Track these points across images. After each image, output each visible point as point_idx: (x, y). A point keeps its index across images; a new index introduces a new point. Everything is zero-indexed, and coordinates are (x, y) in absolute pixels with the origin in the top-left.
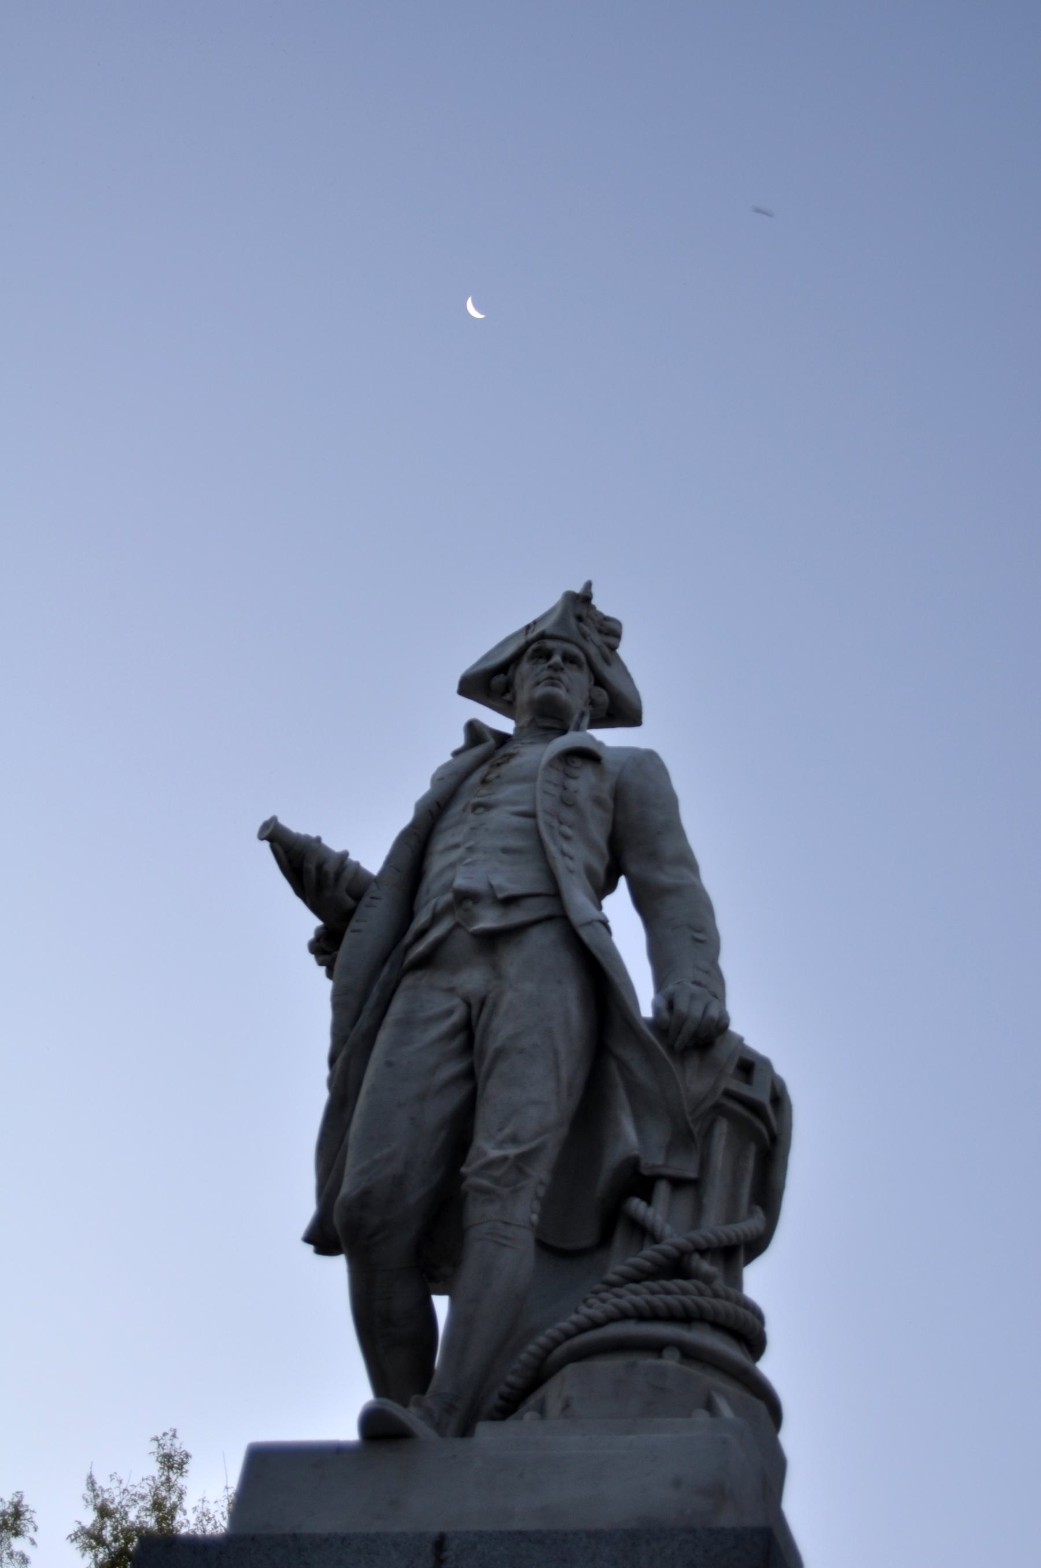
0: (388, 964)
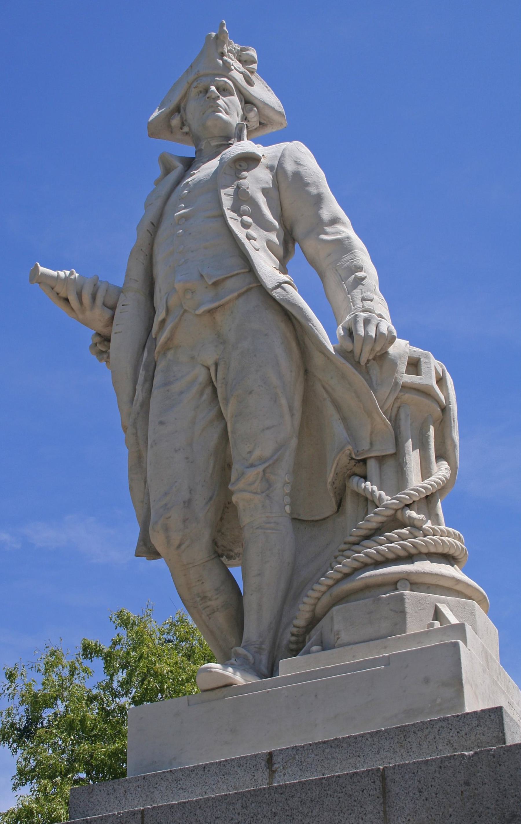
0: (146, 350)
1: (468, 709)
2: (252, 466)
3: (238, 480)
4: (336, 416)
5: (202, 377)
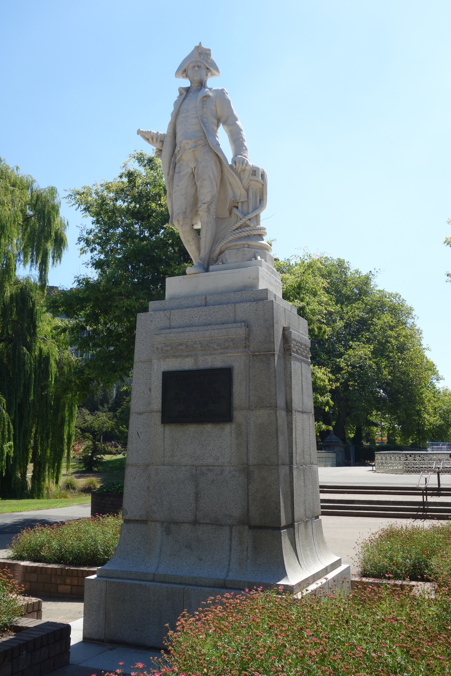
1: (260, 288)
2: (204, 203)
3: (200, 207)
4: (230, 188)
5: (190, 171)
